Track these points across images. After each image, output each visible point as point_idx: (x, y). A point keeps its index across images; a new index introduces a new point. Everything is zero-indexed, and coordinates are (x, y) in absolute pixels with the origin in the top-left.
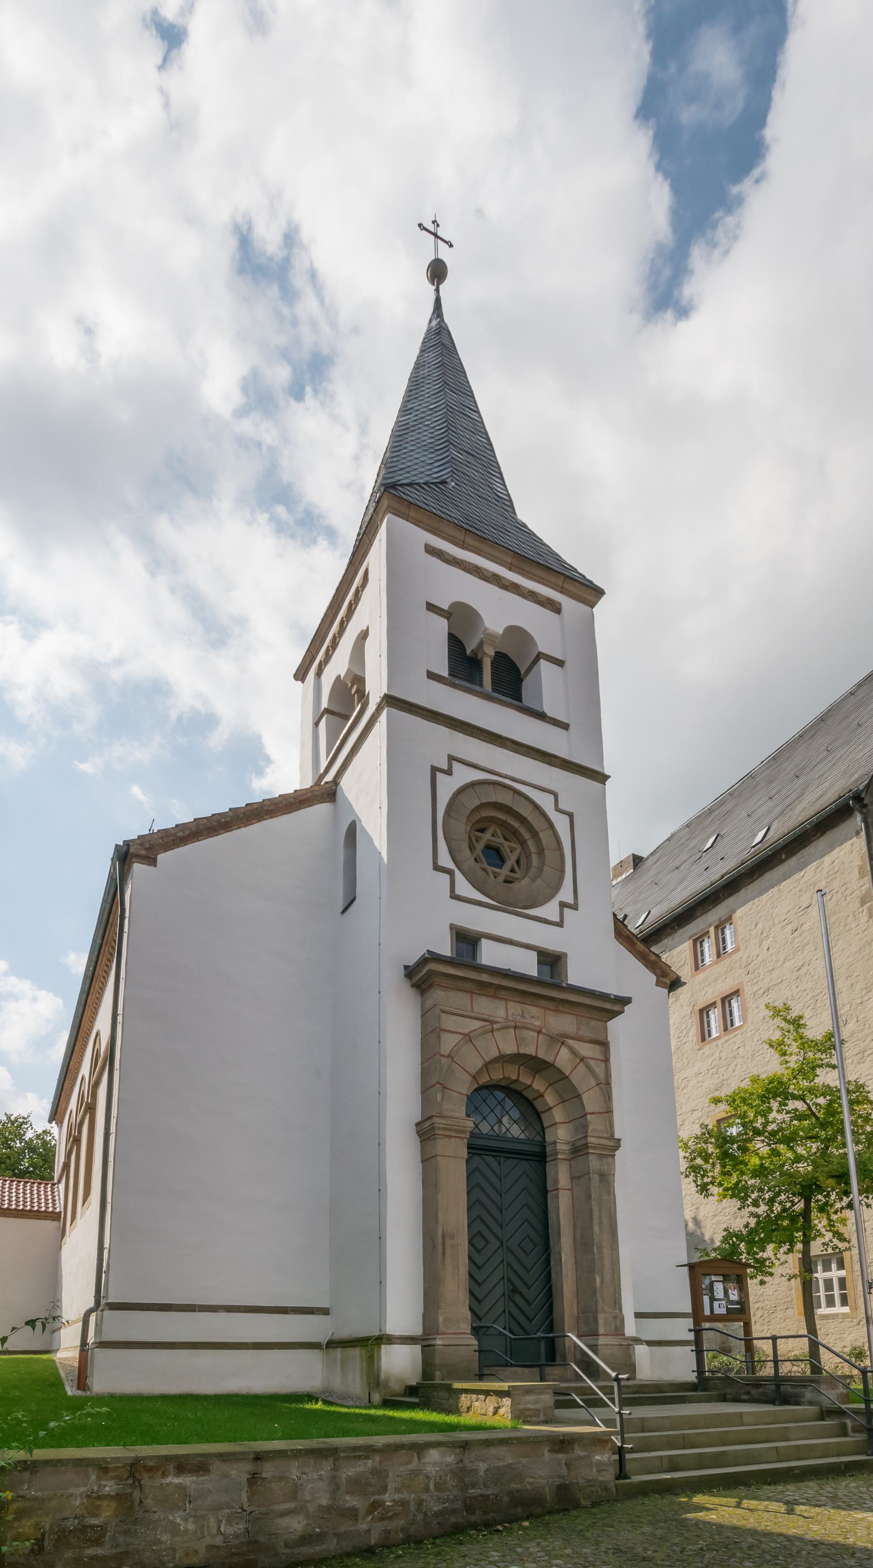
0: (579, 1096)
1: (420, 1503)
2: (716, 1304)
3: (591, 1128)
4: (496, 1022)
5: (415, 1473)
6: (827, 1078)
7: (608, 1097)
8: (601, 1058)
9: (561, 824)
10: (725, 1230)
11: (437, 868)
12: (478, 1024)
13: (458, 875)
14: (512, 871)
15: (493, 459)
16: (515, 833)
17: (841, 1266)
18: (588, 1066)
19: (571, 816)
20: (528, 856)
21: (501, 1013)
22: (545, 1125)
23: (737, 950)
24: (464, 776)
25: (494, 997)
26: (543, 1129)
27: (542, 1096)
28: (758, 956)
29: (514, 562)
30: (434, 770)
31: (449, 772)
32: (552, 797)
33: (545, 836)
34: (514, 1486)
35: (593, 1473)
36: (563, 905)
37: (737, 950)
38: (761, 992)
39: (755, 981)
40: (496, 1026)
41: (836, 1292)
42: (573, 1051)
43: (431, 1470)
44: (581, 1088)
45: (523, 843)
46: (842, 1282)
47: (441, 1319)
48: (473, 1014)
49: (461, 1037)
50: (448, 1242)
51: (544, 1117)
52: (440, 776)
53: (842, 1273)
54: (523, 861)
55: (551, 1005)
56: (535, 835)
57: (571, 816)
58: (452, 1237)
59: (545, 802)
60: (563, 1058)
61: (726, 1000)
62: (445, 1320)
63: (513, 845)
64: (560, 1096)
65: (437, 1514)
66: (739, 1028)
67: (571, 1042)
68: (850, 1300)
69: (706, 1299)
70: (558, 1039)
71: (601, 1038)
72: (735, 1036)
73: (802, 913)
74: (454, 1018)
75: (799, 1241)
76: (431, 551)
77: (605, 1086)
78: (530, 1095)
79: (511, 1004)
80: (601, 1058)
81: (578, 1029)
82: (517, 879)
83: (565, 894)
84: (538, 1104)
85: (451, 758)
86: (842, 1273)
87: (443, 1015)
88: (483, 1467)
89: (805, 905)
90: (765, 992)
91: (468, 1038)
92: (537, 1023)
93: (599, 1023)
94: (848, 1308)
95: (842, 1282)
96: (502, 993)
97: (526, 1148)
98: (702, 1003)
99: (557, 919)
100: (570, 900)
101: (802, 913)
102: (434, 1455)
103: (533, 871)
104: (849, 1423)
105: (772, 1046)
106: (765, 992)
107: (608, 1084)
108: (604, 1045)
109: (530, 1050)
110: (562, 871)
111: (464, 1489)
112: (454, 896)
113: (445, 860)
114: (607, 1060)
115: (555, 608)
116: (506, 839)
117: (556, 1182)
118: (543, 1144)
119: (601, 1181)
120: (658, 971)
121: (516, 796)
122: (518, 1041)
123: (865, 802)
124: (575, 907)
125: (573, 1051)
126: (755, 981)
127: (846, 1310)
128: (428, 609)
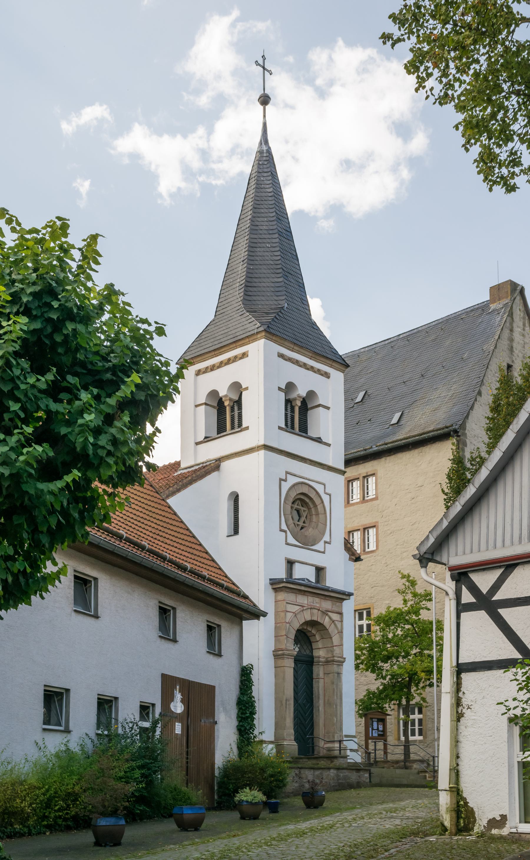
0: (331, 638)
1: (330, 783)
2: (374, 731)
3: (335, 652)
4: (304, 606)
5: (328, 775)
6: (424, 615)
7: (341, 638)
8: (340, 620)
9: (325, 498)
10: (367, 690)
11: (281, 530)
12: (298, 607)
13: (288, 533)
14: (304, 522)
15: (298, 271)
16: (306, 504)
17: (420, 712)
18: (335, 625)
19: (330, 495)
20: (311, 515)
21: (306, 602)
22: (313, 648)
23: (376, 499)
24: (292, 480)
25: (304, 595)
26: (312, 649)
27: (315, 636)
28: (389, 507)
29: (313, 356)
30: (281, 480)
31: (285, 480)
32: (323, 486)
33: (320, 507)
34: (348, 781)
35: (364, 779)
36: (326, 542)
37: (376, 499)
38: (389, 532)
39: (386, 523)
40: (304, 608)
41: (417, 727)
42: (330, 618)
43: (332, 774)
44: (332, 635)
45: (309, 509)
46: (420, 721)
47: (285, 734)
48: (297, 603)
49: (292, 614)
50: (287, 703)
51: (313, 644)
52: (282, 482)
53: (421, 716)
54: (308, 517)
55: (323, 597)
56: (315, 506)
57: (330, 495)
58: (289, 701)
59: (320, 488)
60: (326, 622)
61: (366, 529)
62: (287, 734)
63: (305, 509)
64: (322, 636)
65: (333, 786)
66: (372, 552)
67: (329, 613)
68: (423, 733)
69: (370, 729)
70: (325, 613)
71: (340, 611)
72: (370, 557)
73: (417, 489)
74: (290, 605)
75: (72, 408)
76: (281, 356)
77: (341, 632)
78: (309, 634)
79: (309, 597)
80: (340, 620)
81: (332, 607)
82: (306, 527)
83: (326, 538)
84: (312, 639)
85: (287, 473)
86: (421, 716)
87: (288, 605)
88: (342, 775)
89: (419, 485)
90: (391, 533)
91: (295, 614)
92: (318, 605)
93: (340, 604)
94: (422, 737)
95: (420, 721)
96: (307, 594)
97: (303, 658)
98: (350, 528)
99: (323, 550)
100: (328, 540)
101: (417, 489)
102: (332, 771)
103: (313, 524)
104: (427, 775)
105: (399, 592)
106: (391, 533)
107: (342, 632)
108: (341, 614)
109: (315, 618)
110: (326, 525)
111: (338, 780)
112: (287, 544)
113: (284, 527)
114: (342, 621)
115: (327, 375)
116: (302, 506)
117: (318, 675)
118: (312, 657)
119: (338, 676)
120: (350, 552)
121: (310, 488)
122: (312, 614)
123: (459, 434)
124: (329, 543)
125: (330, 618)
126: (386, 523)
127: (421, 738)
128: (279, 390)
